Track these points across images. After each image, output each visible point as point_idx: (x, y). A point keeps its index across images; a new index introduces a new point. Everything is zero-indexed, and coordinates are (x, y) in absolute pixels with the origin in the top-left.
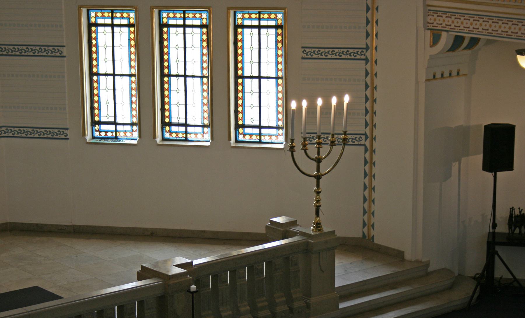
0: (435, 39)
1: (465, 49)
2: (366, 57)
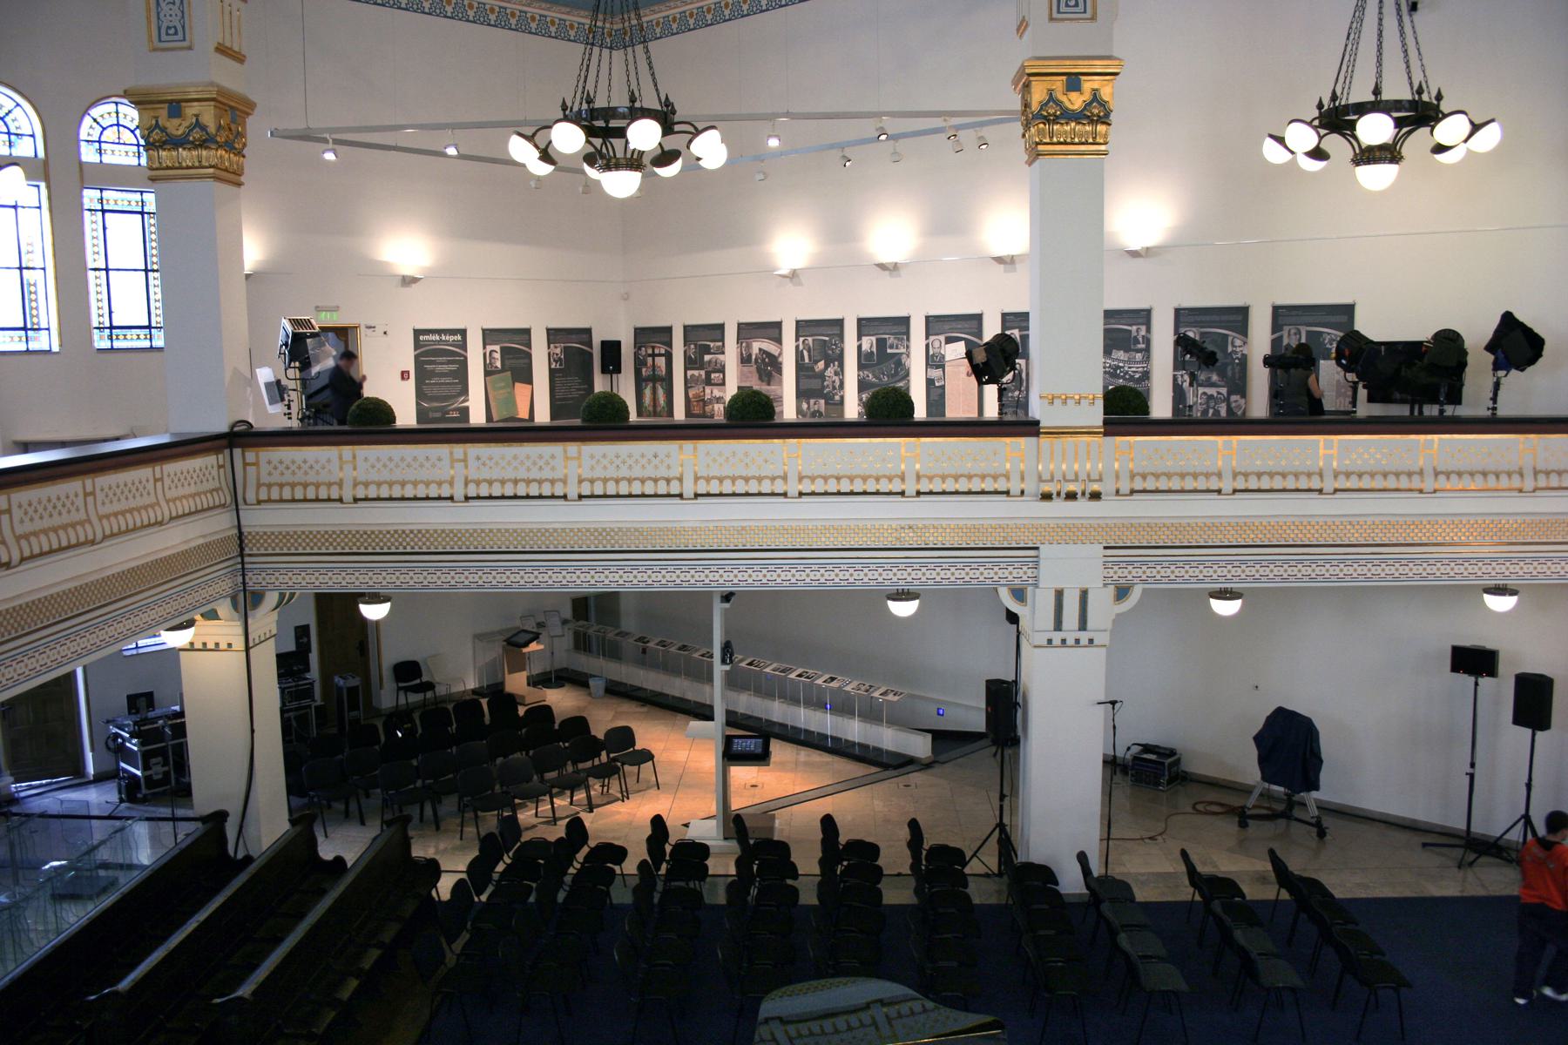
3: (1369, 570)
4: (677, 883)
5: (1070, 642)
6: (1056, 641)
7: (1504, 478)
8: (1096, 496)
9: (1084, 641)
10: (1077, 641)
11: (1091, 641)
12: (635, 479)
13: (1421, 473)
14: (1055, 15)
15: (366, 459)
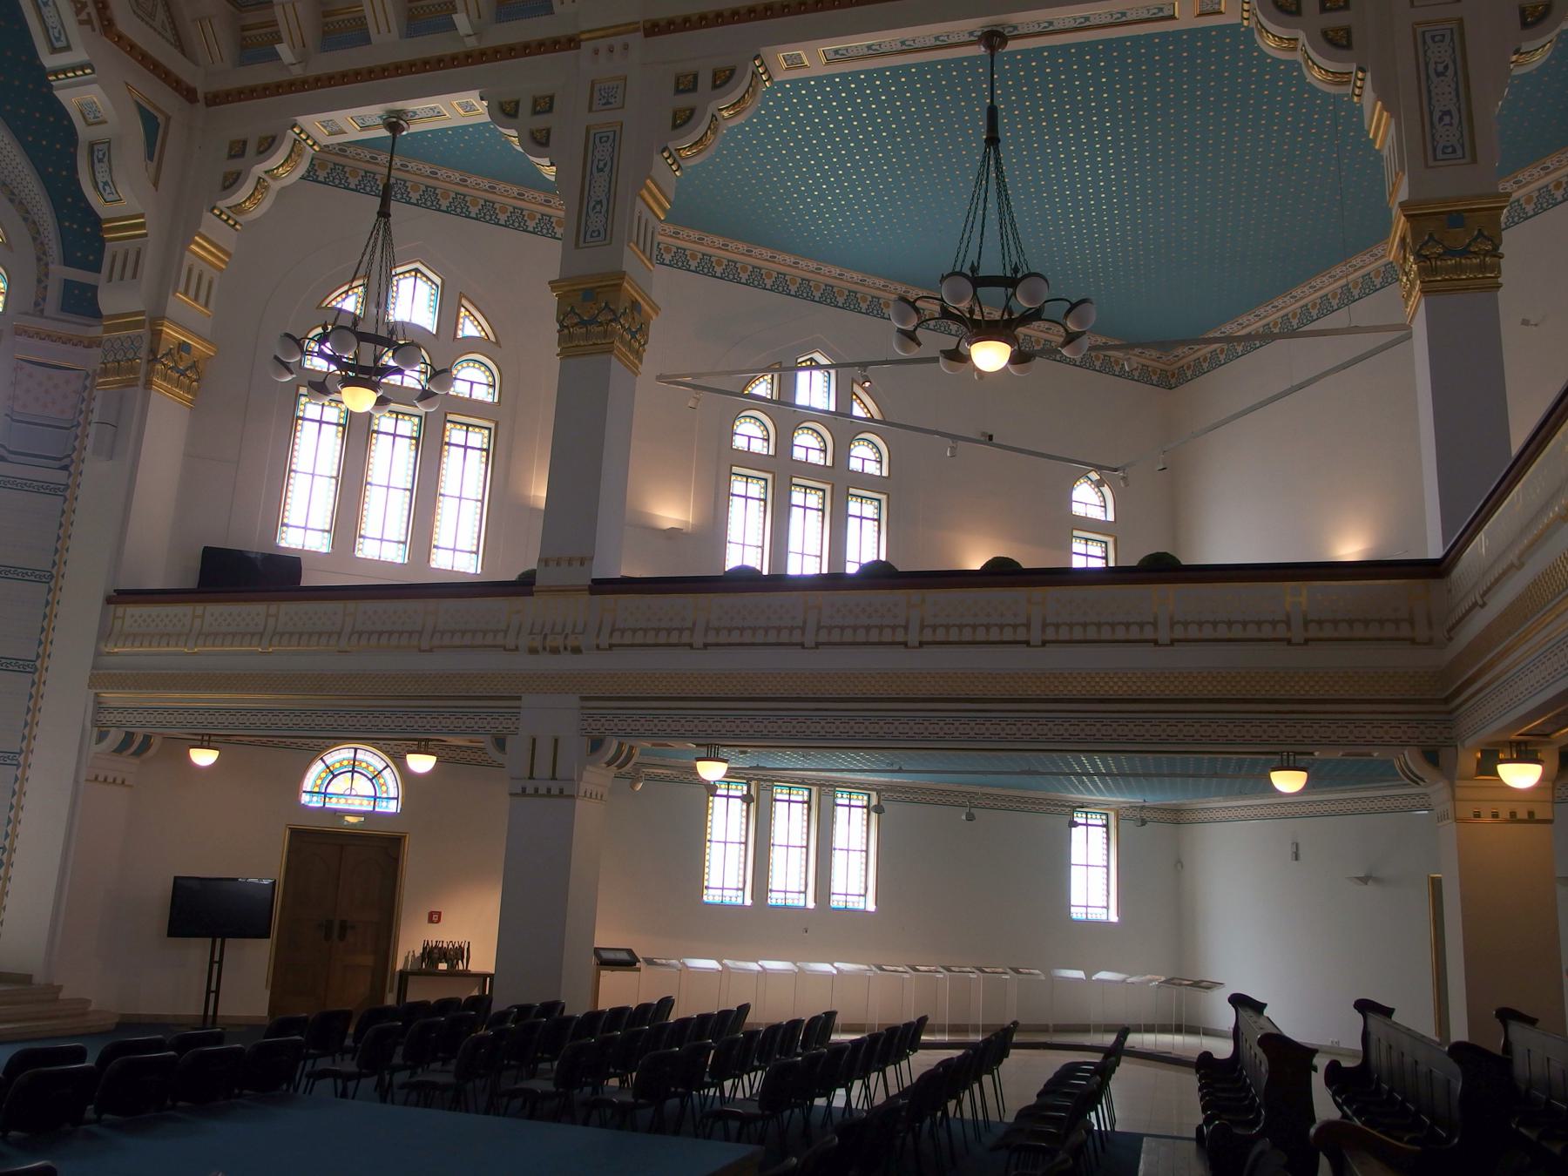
0: (102, 737)
1: (134, 754)
2: (19, 762)
3: (926, 729)
4: (845, 1056)
5: (543, 791)
6: (530, 790)
7: (888, 632)
8: (577, 650)
9: (555, 791)
10: (549, 790)
11: (561, 791)
12: (674, 629)
13: (421, 633)
14: (1431, 162)
15: (133, 616)
